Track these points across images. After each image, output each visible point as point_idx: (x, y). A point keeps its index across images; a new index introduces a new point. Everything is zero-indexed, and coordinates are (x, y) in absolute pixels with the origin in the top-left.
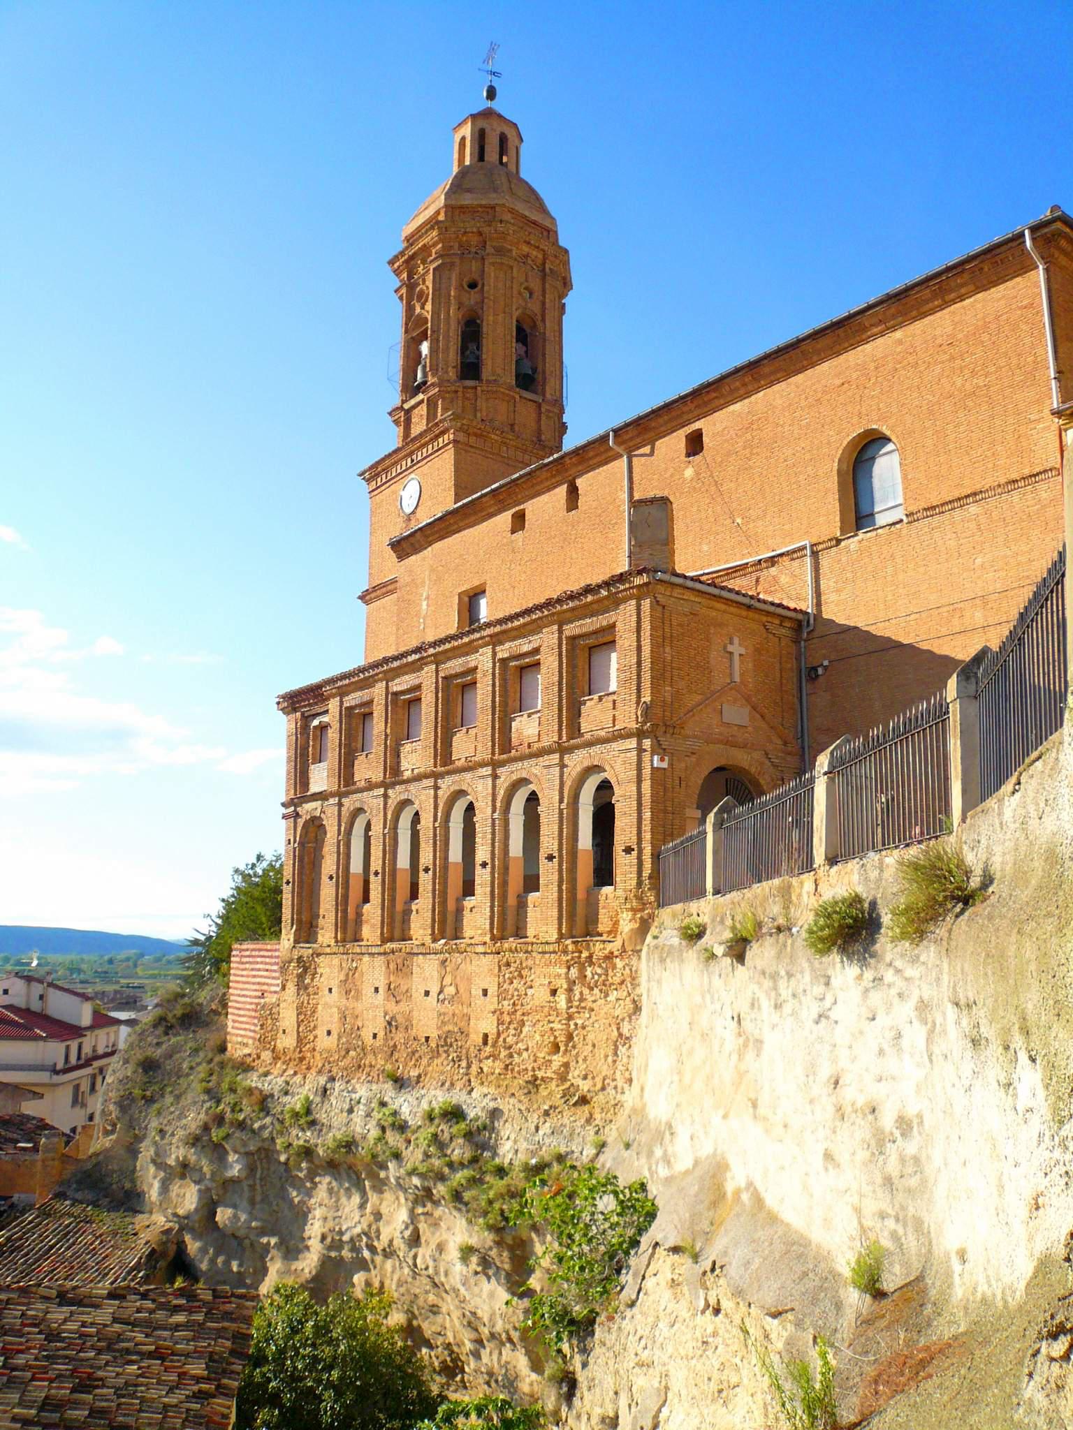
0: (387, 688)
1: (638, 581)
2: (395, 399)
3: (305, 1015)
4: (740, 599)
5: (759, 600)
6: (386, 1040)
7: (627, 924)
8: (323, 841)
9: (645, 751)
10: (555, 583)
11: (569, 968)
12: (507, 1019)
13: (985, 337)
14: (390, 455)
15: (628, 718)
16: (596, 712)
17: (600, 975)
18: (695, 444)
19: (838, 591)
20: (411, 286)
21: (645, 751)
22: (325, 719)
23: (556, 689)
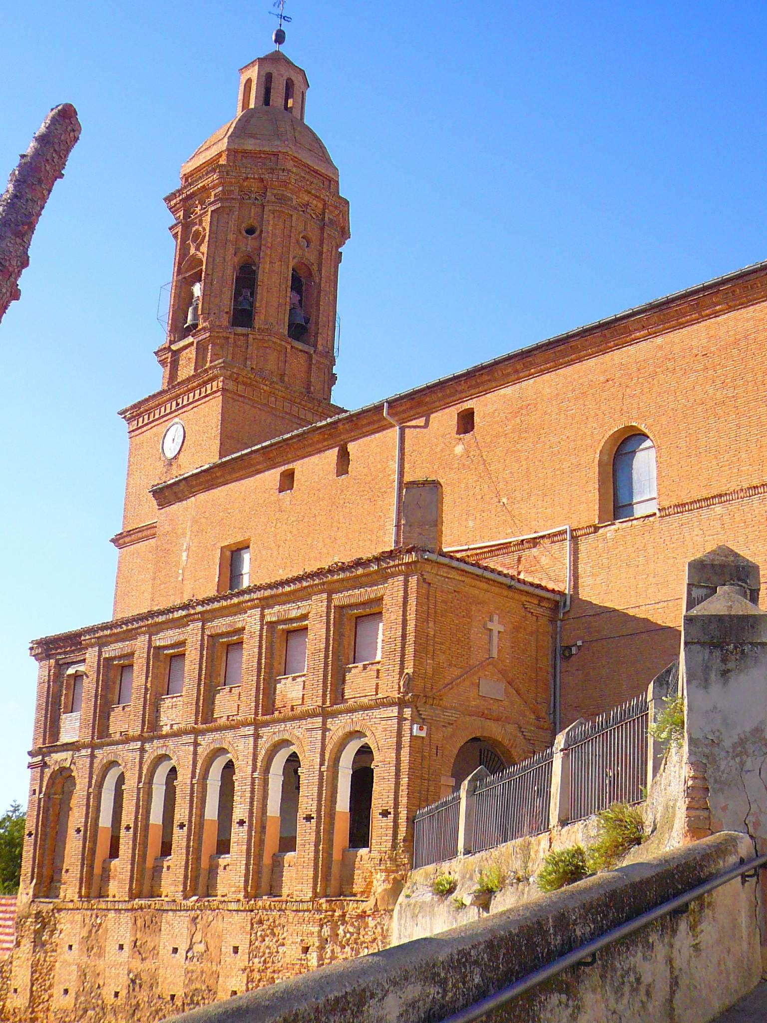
0: (150, 641)
1: (407, 559)
2: (162, 337)
3: (40, 974)
4: (501, 579)
5: (519, 581)
6: (128, 998)
7: (380, 885)
8: (72, 792)
9: (406, 719)
10: (320, 545)
11: (321, 926)
12: (257, 976)
13: (735, 352)
14: (154, 396)
15: (391, 687)
16: (360, 680)
17: (352, 934)
18: (466, 422)
19: (593, 575)
20: (186, 225)
21: (406, 719)
22: (81, 668)
23: (322, 655)
